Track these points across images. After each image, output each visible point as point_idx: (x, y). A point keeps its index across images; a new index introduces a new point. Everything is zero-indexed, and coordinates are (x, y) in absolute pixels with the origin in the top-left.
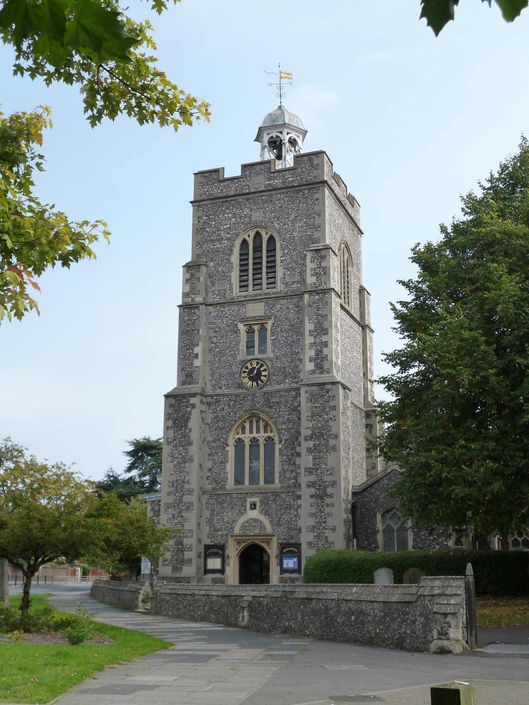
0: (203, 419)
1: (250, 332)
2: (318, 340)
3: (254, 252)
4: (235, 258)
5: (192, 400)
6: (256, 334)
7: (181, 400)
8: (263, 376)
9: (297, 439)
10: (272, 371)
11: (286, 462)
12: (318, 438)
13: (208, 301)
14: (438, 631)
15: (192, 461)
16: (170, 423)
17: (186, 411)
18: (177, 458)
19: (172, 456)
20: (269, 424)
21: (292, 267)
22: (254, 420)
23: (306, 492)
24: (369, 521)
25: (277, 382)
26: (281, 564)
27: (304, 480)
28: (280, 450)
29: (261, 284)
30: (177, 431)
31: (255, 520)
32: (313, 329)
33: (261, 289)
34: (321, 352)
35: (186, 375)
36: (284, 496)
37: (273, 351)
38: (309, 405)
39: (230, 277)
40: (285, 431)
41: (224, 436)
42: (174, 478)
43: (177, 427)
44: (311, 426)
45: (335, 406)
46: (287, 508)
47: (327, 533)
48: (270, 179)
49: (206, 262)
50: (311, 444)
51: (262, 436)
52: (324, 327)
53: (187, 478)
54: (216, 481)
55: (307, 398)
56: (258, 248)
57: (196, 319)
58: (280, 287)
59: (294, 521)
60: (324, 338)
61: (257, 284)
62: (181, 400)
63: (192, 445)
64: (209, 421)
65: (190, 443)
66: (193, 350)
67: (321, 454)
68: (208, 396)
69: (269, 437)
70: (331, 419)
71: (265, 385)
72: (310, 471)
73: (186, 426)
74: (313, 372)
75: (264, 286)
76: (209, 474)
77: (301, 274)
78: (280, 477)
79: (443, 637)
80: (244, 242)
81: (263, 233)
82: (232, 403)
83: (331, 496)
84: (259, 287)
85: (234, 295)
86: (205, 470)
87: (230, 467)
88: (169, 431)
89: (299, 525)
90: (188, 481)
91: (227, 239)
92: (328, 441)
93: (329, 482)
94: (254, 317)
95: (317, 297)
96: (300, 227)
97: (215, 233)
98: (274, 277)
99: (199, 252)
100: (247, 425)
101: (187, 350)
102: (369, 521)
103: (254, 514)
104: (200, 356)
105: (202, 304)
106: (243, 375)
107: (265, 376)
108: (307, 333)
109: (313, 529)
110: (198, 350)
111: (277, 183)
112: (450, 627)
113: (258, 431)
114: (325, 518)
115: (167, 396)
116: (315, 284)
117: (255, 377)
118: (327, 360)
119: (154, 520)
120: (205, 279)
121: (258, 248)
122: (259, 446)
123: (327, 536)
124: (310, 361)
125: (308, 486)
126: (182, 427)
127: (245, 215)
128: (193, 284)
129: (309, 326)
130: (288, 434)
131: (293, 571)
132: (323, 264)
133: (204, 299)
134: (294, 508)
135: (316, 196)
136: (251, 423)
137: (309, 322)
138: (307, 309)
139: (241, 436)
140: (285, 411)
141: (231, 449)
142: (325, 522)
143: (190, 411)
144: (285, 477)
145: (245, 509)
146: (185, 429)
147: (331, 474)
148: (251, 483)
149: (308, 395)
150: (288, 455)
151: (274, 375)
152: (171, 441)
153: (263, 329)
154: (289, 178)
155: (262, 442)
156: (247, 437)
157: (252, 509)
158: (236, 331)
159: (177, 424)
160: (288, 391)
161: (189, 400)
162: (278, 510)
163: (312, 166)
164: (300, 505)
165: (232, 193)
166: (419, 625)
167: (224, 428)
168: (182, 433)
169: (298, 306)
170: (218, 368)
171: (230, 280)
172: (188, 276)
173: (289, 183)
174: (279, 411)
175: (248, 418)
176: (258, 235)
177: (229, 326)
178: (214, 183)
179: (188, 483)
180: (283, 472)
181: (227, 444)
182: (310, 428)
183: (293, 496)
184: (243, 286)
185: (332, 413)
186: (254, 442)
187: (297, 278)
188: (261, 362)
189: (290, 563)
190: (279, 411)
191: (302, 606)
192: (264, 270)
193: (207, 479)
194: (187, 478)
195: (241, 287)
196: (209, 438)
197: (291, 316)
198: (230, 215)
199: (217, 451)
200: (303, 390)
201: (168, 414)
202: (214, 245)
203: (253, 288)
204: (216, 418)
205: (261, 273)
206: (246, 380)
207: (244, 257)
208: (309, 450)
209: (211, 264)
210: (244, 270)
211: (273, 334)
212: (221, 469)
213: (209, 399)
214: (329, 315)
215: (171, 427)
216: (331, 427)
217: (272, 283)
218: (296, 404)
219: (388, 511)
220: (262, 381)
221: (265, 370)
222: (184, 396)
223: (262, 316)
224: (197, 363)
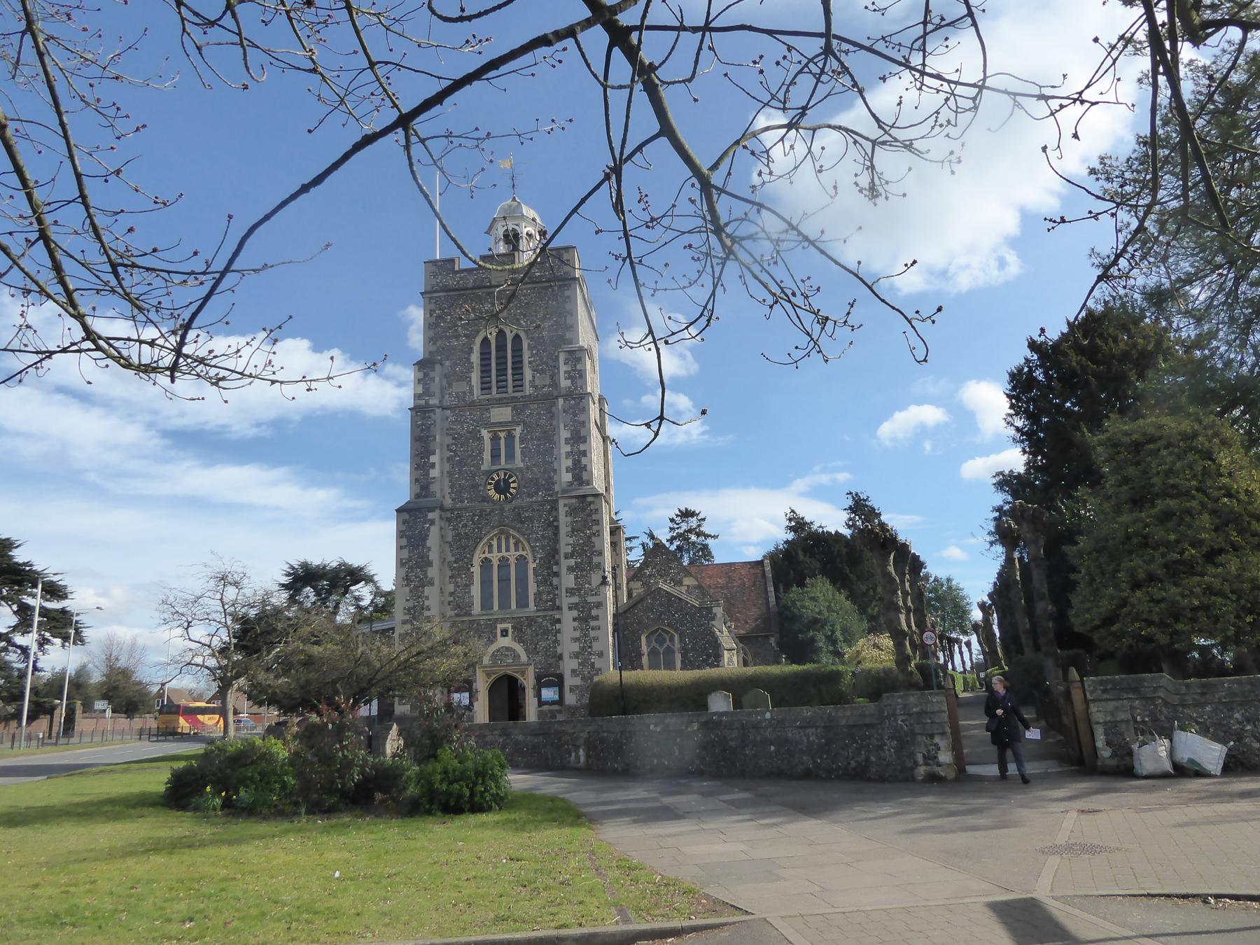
0: (442, 536)
1: (495, 439)
2: (575, 449)
3: (497, 351)
4: (475, 358)
5: (431, 516)
6: (502, 442)
9: (553, 557)
11: (542, 582)
13: (445, 404)
14: (924, 755)
15: (432, 584)
16: (404, 542)
18: (413, 581)
19: (407, 579)
20: (520, 541)
22: (503, 537)
23: (568, 616)
24: (632, 644)
26: (539, 695)
27: (566, 601)
28: (534, 569)
29: (506, 387)
31: (508, 649)
32: (569, 436)
33: (507, 392)
34: (579, 461)
35: (421, 487)
37: (523, 461)
38: (569, 519)
42: (410, 604)
43: (413, 546)
46: (544, 633)
47: (594, 659)
49: (441, 360)
50: (572, 562)
51: (512, 555)
52: (582, 435)
54: (459, 607)
56: (501, 347)
57: (432, 424)
58: (528, 390)
59: (553, 647)
60: (582, 447)
61: (502, 386)
64: (450, 539)
65: (430, 564)
66: (429, 459)
67: (584, 573)
68: (448, 510)
69: (521, 556)
70: (594, 534)
71: (514, 497)
72: (571, 592)
73: (424, 546)
74: (571, 484)
75: (510, 389)
76: (452, 599)
77: (552, 377)
78: (535, 600)
79: (931, 762)
80: (486, 341)
81: (507, 331)
83: (596, 618)
84: (520, 388)
85: (475, 398)
86: (447, 594)
87: (476, 590)
89: (559, 651)
90: (428, 606)
91: (465, 335)
93: (594, 603)
94: (500, 423)
95: (573, 402)
97: (450, 329)
98: (522, 380)
99: (433, 348)
100: (495, 543)
101: (421, 459)
102: (632, 644)
103: (506, 642)
104: (437, 466)
105: (439, 407)
106: (489, 487)
107: (514, 488)
108: (563, 442)
109: (576, 655)
110: (434, 459)
112: (939, 749)
113: (508, 550)
114: (591, 643)
115: (398, 511)
116: (570, 388)
117: (502, 488)
120: (441, 379)
121: (501, 347)
122: (509, 565)
123: (594, 663)
125: (570, 609)
126: (418, 545)
128: (426, 384)
129: (564, 434)
131: (553, 703)
132: (579, 367)
133: (440, 402)
135: (567, 293)
136: (499, 540)
139: (487, 555)
141: (476, 570)
142: (590, 647)
143: (429, 528)
144: (541, 599)
145: (495, 637)
146: (423, 548)
147: (596, 594)
148: (500, 607)
149: (567, 509)
151: (525, 487)
153: (510, 437)
155: (512, 561)
156: (495, 557)
157: (502, 636)
158: (481, 439)
160: (543, 503)
164: (559, 629)
165: (470, 285)
166: (889, 750)
167: (468, 546)
170: (457, 479)
171: (470, 381)
172: (420, 375)
173: (536, 277)
174: (532, 526)
175: (495, 535)
176: (501, 334)
177: (470, 433)
178: (448, 274)
179: (428, 609)
180: (538, 595)
181: (472, 565)
184: (485, 387)
185: (595, 528)
186: (504, 562)
187: (548, 381)
188: (509, 473)
189: (549, 694)
190: (532, 526)
191: (678, 740)
192: (510, 371)
193: (449, 604)
194: (426, 603)
195: (482, 389)
196: (451, 558)
197: (542, 422)
200: (561, 503)
201: (401, 532)
204: (458, 535)
205: (506, 375)
206: (492, 492)
207: (485, 356)
208: (570, 569)
209: (447, 363)
210: (485, 370)
211: (522, 442)
212: (466, 592)
213: (449, 515)
215: (405, 546)
217: (519, 385)
219: (652, 633)
220: (511, 494)
221: (514, 482)
222: (418, 509)
223: (510, 422)
224: (434, 473)
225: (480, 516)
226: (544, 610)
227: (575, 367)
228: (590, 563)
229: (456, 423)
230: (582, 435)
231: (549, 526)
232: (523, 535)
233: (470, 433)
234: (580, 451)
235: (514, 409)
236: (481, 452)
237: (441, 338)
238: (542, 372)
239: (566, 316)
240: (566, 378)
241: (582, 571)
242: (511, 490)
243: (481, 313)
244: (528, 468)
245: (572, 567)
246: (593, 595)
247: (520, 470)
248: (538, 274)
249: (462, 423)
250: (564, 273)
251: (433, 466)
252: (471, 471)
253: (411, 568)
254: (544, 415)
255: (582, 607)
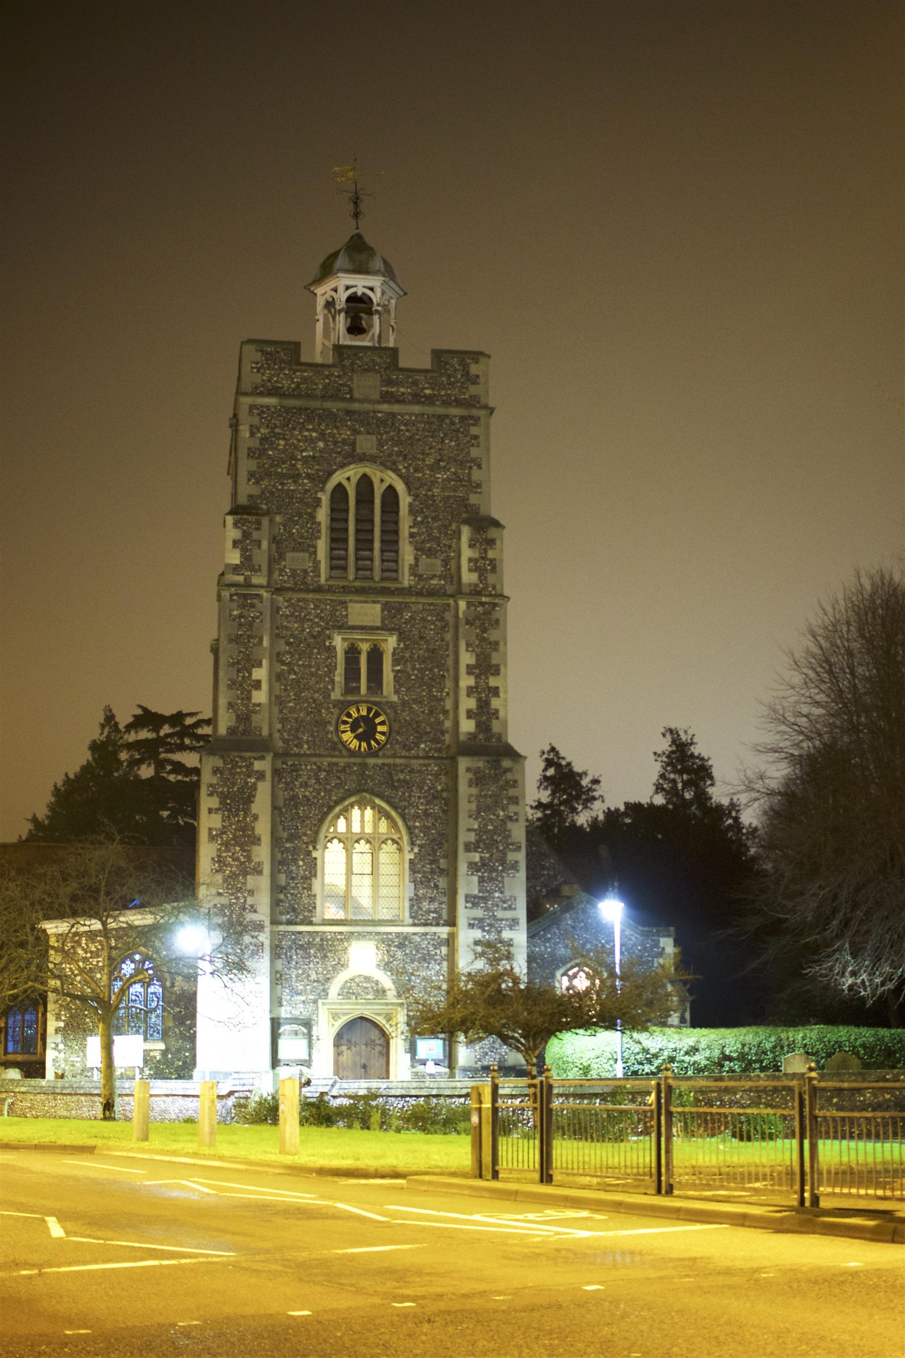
4: (323, 515)
7: (237, 762)
8: (381, 733)
10: (396, 726)
11: (422, 882)
12: (488, 848)
17: (247, 783)
19: (219, 862)
21: (430, 549)
25: (405, 745)
30: (229, 817)
34: (487, 703)
36: (419, 940)
37: (397, 692)
38: (474, 791)
39: (315, 547)
40: (420, 831)
41: (309, 832)
43: (229, 810)
44: (476, 827)
45: (517, 798)
48: (390, 383)
50: (476, 857)
52: (494, 662)
53: (250, 901)
54: (294, 910)
55: (470, 781)
57: (258, 617)
60: (493, 682)
62: (237, 762)
63: (260, 845)
65: (257, 841)
66: (250, 674)
67: (494, 875)
73: (247, 811)
82: (323, 775)
88: (213, 816)
90: (252, 906)
92: (505, 855)
95: (480, 609)
96: (444, 480)
101: (239, 671)
106: (342, 727)
107: (383, 733)
110: (260, 674)
111: (403, 394)
116: (476, 585)
118: (497, 718)
119: (64, 969)
124: (469, 717)
125: (471, 926)
126: (238, 810)
127: (344, 439)
128: (247, 550)
129: (467, 658)
130: (425, 835)
134: (436, 960)
137: (467, 650)
138: (463, 628)
140: (419, 798)
143: (255, 784)
147: (510, 908)
150: (424, 872)
151: (398, 733)
152: (216, 835)
154: (427, 388)
158: (331, 650)
159: (229, 804)
161: (252, 764)
162: (407, 963)
163: (466, 374)
168: (238, 821)
169: (442, 618)
170: (292, 710)
171: (315, 553)
174: (410, 796)
177: (314, 637)
181: (314, 848)
182: (475, 830)
183: (433, 940)
184: (337, 564)
187: (439, 570)
190: (410, 796)
192: (377, 545)
198: (314, 434)
199: (296, 857)
202: (283, 484)
203: (356, 574)
205: (372, 550)
206: (347, 736)
210: (338, 539)
211: (396, 662)
214: (501, 644)
215: (217, 810)
216: (509, 831)
218: (439, 788)
221: (382, 723)
223: (378, 628)
224: (260, 697)
225: (328, 772)
226: (425, 925)
227: (486, 551)
228: (503, 861)
229: (293, 619)
230: (494, 662)
231: (434, 797)
232: (395, 808)
233: (314, 637)
234: (489, 688)
235: (386, 606)
236: (332, 669)
237: (269, 475)
238: (431, 553)
239: (470, 468)
240: (470, 570)
241: (491, 872)
242: (378, 736)
243: (336, 443)
244: (404, 703)
245: (476, 864)
246: (505, 909)
247: (392, 705)
248: (428, 392)
249: (302, 620)
250: (471, 397)
251: (257, 685)
252: (315, 701)
253: (226, 844)
254: (433, 623)
255: (488, 925)
